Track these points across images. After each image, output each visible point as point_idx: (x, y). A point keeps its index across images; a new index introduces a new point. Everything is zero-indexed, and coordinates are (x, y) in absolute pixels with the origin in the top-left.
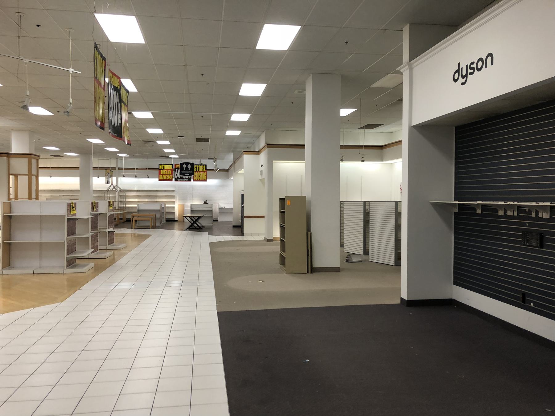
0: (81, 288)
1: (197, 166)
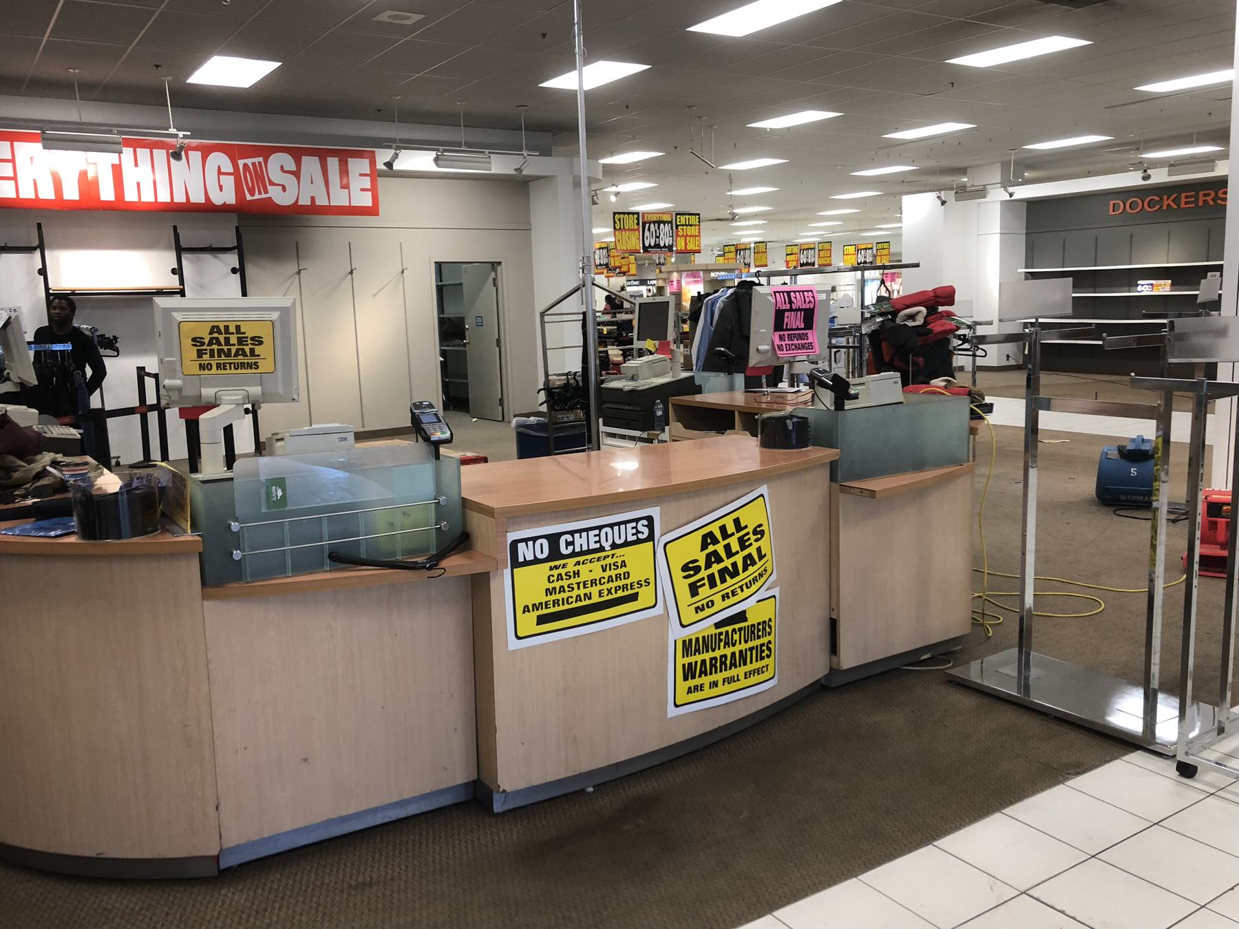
0: (763, 554)
1: (622, 216)
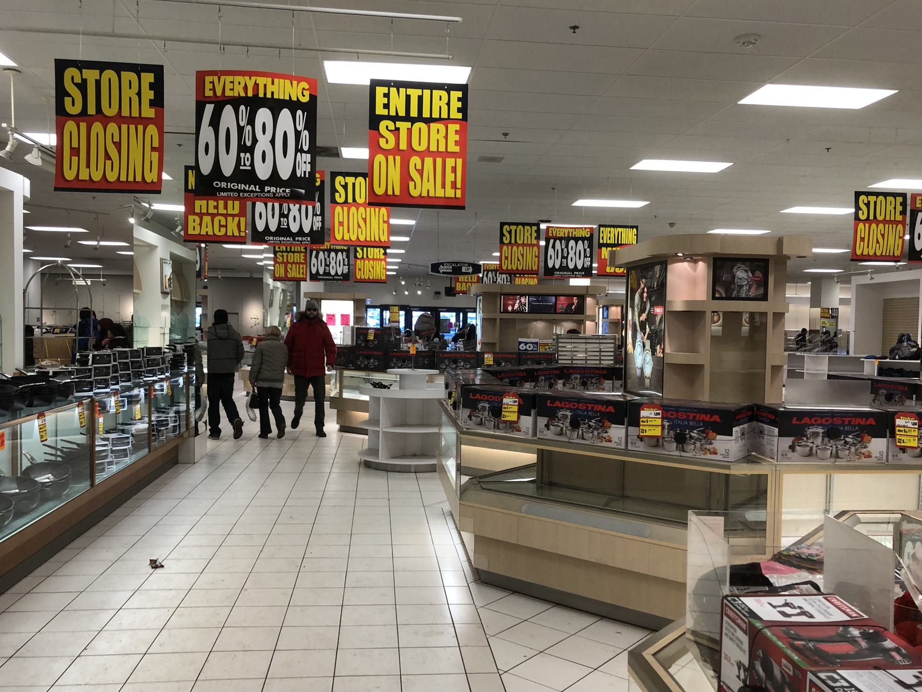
1: (91, 75)
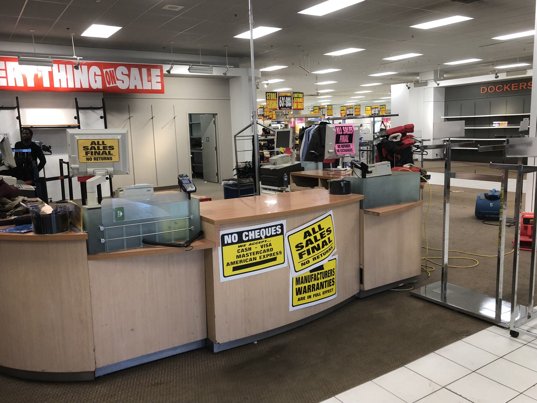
1: (269, 94)
